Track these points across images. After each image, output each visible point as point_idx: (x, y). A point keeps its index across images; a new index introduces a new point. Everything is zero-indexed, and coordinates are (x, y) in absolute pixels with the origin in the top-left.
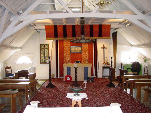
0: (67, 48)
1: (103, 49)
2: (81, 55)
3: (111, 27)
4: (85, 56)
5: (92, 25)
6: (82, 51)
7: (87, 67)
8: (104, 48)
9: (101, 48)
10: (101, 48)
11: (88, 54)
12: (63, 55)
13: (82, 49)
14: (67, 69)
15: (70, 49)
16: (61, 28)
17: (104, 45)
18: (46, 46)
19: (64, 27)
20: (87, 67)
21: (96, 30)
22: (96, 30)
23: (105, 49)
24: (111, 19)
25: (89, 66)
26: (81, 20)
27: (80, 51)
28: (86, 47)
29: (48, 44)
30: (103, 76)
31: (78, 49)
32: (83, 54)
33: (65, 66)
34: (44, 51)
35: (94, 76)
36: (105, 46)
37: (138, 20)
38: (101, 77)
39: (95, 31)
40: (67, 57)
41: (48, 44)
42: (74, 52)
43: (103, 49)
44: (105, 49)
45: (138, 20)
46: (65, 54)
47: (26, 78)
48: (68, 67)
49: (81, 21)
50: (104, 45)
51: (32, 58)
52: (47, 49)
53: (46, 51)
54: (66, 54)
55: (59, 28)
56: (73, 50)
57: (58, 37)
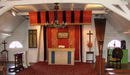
0: (55, 34)
1: (89, 35)
2: (68, 40)
3: (93, 13)
4: (72, 41)
5: (74, 11)
6: (68, 37)
7: (71, 52)
8: (90, 34)
9: (88, 34)
10: (88, 34)
11: (74, 39)
12: (51, 40)
13: (68, 35)
14: (52, 54)
15: (58, 35)
16: (44, 14)
17: (90, 31)
18: (34, 32)
19: (63, 13)
20: (71, 52)
21: (77, 16)
22: (77, 16)
23: (91, 35)
24: (89, 4)
25: (73, 50)
26: (56, 5)
27: (66, 37)
28: (72, 33)
29: (36, 30)
30: (87, 61)
31: (65, 35)
32: (69, 39)
33: (50, 50)
34: (32, 36)
35: (80, 61)
36: (91, 33)
37: (113, 5)
38: (85, 62)
39: (76, 17)
40: (54, 41)
41: (36, 30)
42: (61, 37)
43: (89, 35)
44: (91, 35)
45: (113, 5)
46: (52, 39)
47: (96, 56)
48: (52, 52)
49: (55, 6)
50: (90, 31)
51: (23, 43)
52: (35, 35)
53: (34, 36)
54: (53, 40)
55: (76, 13)
56: (60, 36)
57: (41, 23)
